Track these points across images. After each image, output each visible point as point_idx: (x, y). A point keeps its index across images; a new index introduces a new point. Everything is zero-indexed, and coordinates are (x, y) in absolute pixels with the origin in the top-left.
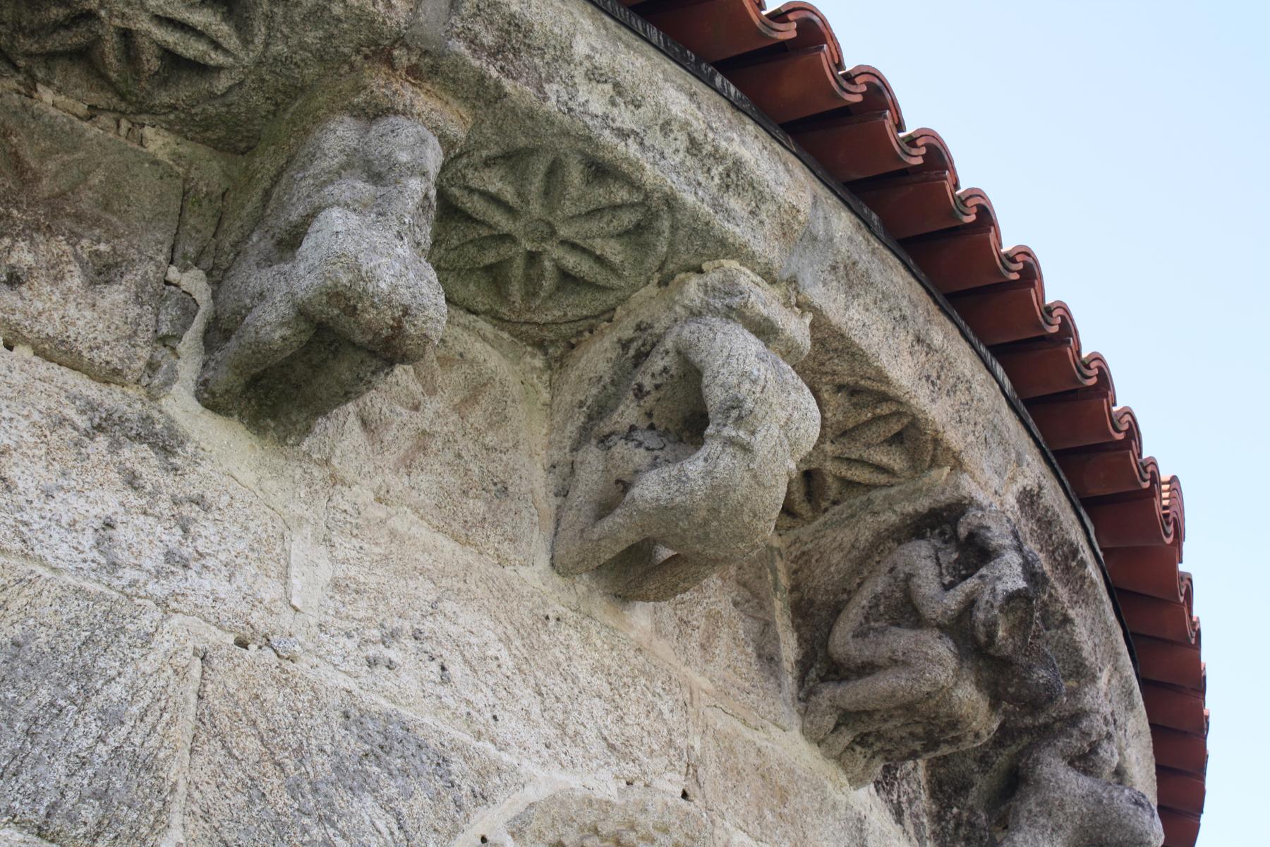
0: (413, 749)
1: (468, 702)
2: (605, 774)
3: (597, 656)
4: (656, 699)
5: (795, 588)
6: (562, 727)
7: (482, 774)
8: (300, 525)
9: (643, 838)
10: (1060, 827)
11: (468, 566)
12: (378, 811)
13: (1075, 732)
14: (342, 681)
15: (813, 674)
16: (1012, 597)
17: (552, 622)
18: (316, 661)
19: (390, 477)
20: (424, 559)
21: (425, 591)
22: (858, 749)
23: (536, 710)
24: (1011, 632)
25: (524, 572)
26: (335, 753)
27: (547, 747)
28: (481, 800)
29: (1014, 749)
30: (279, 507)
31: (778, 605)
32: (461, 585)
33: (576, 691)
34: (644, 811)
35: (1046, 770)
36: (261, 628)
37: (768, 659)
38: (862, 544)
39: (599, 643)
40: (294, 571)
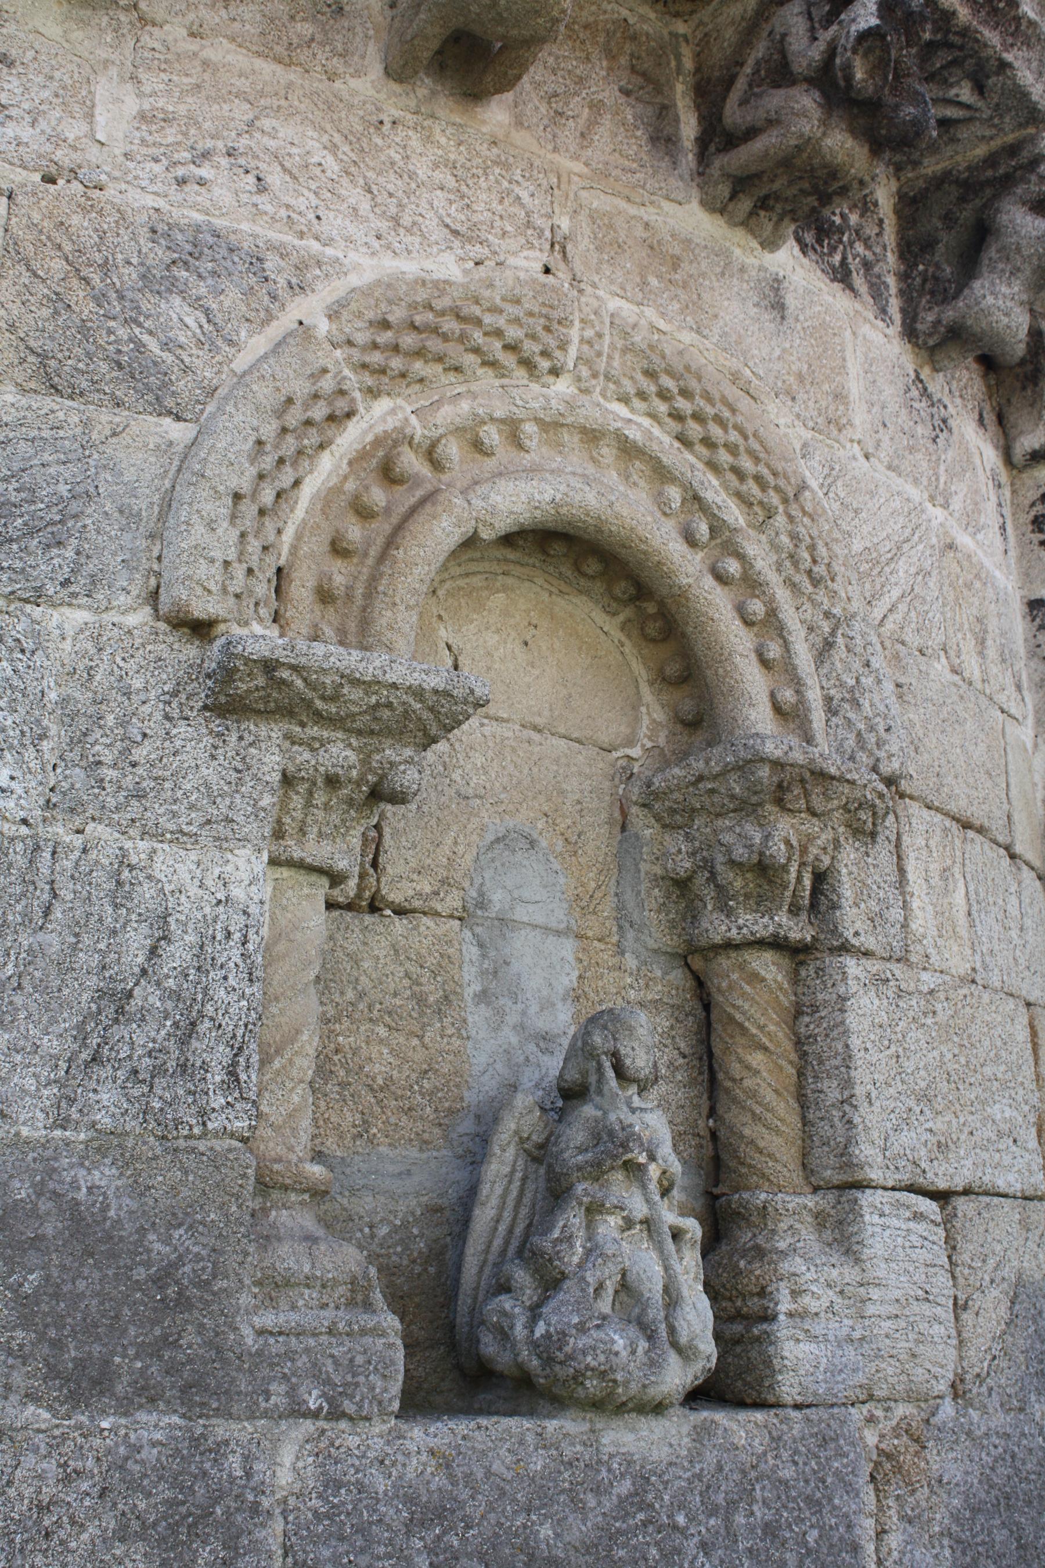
0: (224, 252)
1: (288, 206)
2: (448, 258)
3: (440, 152)
4: (514, 186)
5: (698, 70)
6: (396, 220)
7: (301, 268)
8: (106, 68)
9: (489, 310)
10: (1019, 270)
11: (290, 85)
12: (187, 309)
13: (1033, 178)
14: (150, 201)
15: (712, 148)
16: (864, 36)
17: (387, 126)
18: (124, 186)
19: (203, 12)
20: (241, 84)
21: (242, 112)
22: (762, 213)
23: (365, 206)
24: (871, 74)
25: (354, 83)
26: (142, 264)
27: (378, 238)
28: (297, 290)
29: (978, 202)
30: (86, 54)
31: (680, 88)
32: (283, 102)
33: (413, 186)
34: (491, 286)
35: (1005, 217)
36: (67, 163)
37: (663, 139)
38: (750, 13)
39: (443, 141)
40: (97, 111)
